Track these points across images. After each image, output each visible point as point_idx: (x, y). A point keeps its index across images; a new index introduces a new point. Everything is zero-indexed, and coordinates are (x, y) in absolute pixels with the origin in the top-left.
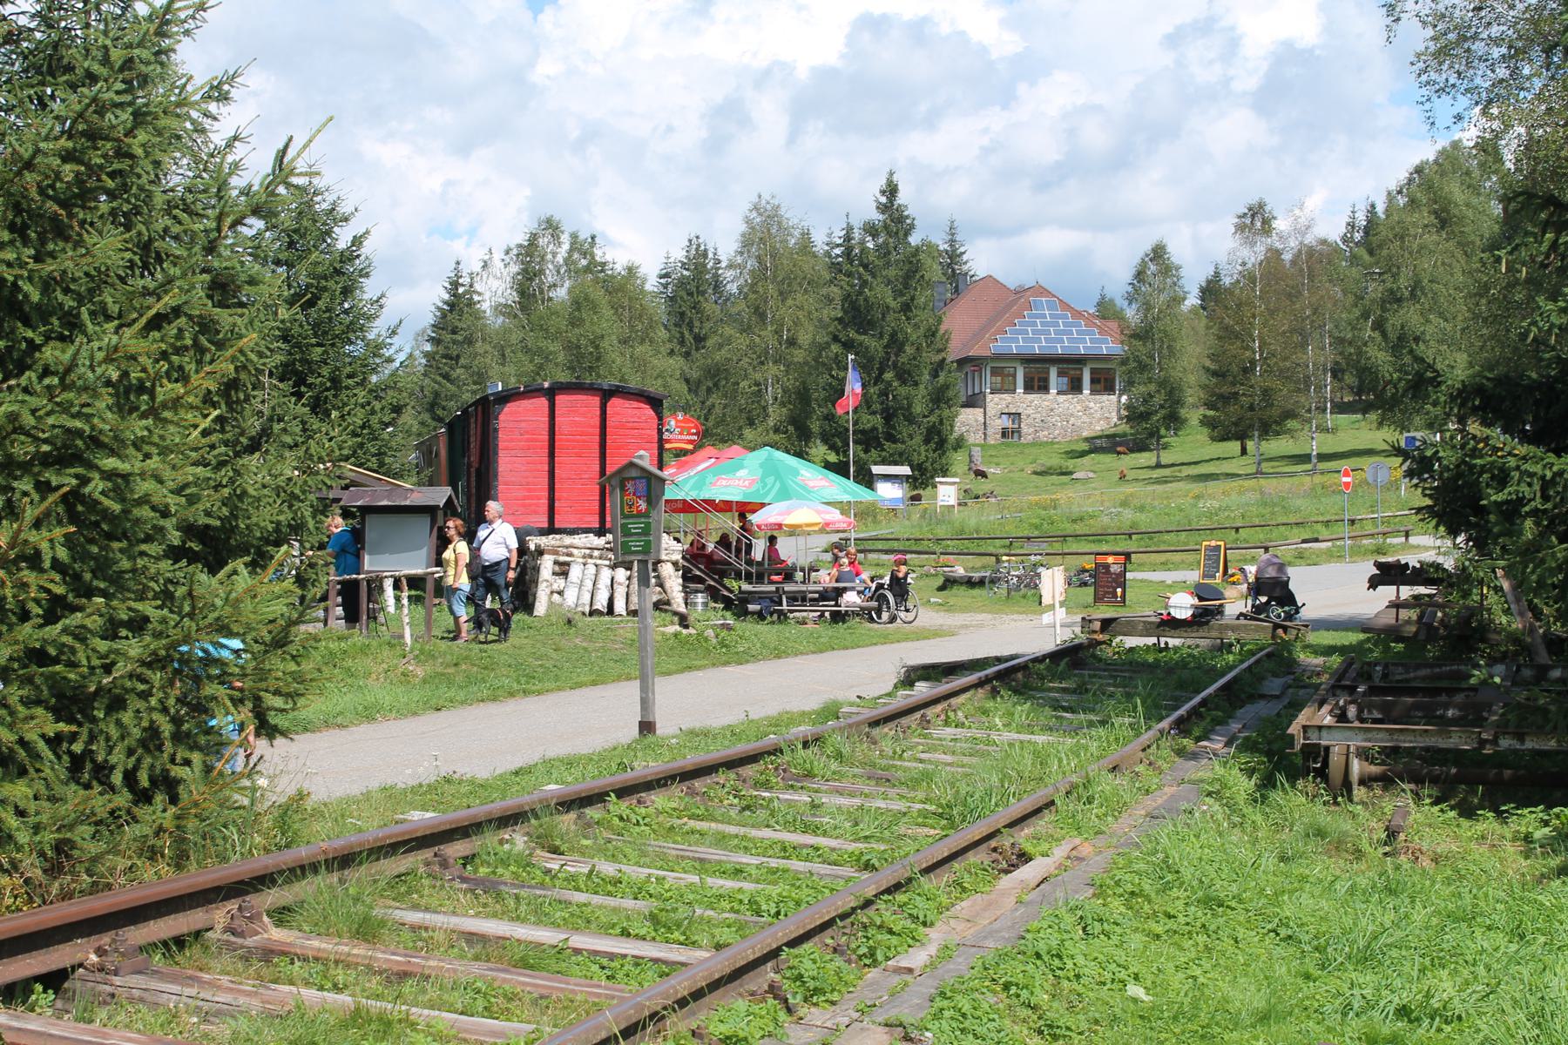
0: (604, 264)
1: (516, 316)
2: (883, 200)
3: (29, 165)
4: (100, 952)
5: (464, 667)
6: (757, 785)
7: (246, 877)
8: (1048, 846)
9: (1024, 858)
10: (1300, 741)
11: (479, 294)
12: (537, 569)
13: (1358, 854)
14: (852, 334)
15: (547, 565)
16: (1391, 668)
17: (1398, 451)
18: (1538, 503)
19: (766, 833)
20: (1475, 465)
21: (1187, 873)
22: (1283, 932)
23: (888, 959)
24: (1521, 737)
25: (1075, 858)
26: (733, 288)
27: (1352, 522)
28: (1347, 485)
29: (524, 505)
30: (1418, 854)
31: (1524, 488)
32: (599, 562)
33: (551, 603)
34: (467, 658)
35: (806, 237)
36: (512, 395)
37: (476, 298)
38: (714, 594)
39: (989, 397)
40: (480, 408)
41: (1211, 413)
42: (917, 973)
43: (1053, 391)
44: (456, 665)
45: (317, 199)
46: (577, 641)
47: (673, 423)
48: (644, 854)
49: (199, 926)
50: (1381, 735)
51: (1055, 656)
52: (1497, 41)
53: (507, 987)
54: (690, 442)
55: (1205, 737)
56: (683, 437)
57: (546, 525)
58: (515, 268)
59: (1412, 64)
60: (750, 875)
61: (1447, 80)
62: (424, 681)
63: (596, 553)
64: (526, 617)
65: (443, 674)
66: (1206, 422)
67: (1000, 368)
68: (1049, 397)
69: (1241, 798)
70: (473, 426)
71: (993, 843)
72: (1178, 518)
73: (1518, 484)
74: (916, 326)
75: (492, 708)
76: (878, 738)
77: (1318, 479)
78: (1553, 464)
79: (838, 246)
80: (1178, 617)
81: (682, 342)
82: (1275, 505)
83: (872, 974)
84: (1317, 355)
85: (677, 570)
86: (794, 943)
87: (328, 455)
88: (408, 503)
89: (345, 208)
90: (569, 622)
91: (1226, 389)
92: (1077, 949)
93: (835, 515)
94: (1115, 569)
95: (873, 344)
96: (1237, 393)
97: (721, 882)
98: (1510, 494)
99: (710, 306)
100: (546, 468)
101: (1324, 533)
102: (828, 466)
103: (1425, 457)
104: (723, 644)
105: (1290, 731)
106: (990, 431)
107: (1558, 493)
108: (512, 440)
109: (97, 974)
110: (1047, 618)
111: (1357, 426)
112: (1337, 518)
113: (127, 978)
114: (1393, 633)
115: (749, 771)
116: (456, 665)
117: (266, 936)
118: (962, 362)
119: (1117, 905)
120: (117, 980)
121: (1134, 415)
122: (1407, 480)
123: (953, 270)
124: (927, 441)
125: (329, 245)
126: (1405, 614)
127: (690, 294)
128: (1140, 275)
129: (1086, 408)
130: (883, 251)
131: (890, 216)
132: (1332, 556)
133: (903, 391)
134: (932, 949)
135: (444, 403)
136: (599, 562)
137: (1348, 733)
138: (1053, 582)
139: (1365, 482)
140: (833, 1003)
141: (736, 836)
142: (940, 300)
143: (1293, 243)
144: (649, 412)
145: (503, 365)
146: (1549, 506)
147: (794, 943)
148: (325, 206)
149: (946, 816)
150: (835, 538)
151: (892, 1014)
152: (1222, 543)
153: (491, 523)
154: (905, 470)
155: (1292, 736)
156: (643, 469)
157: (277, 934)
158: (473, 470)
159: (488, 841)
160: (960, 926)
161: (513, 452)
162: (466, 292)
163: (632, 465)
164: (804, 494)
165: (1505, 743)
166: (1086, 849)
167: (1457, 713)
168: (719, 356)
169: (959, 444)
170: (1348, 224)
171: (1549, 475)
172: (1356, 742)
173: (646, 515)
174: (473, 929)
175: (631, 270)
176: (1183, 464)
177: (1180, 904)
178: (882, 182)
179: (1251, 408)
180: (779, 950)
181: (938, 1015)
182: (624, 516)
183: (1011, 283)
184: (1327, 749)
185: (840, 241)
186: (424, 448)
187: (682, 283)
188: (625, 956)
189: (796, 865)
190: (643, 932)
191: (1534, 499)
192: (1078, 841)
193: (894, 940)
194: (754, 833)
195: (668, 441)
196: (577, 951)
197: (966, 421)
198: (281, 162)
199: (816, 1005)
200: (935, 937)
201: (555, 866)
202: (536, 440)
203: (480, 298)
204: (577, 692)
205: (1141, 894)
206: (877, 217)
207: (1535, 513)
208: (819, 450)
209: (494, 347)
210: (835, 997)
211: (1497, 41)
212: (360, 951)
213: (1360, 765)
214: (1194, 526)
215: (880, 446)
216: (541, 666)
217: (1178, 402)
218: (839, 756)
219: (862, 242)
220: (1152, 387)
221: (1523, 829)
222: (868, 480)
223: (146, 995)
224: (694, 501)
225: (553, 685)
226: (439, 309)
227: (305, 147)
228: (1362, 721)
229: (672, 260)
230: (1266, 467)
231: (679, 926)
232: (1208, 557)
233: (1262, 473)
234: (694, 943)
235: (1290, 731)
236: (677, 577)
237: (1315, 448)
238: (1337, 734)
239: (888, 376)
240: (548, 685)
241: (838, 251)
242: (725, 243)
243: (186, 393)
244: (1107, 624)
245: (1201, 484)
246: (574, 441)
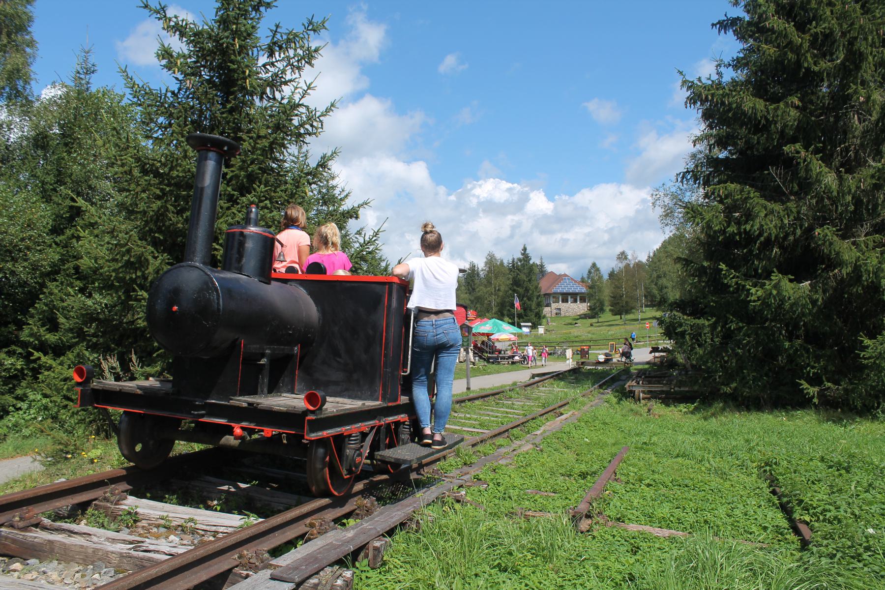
6: (499, 399)
9: (562, 414)
13: (641, 415)
14: (515, 288)
17: (658, 319)
18: (689, 331)
21: (599, 417)
26: (482, 276)
27: (649, 337)
35: (502, 263)
38: (480, 357)
51: (569, 371)
52: (680, 213)
55: (606, 389)
66: (611, 310)
67: (555, 296)
81: (469, 290)
84: (640, 292)
86: (512, 428)
91: (616, 302)
93: (513, 336)
94: (586, 350)
95: (521, 290)
101: (642, 340)
102: (509, 323)
104: (484, 370)
110: (568, 362)
114: (654, 364)
115: (497, 396)
118: (545, 295)
121: (591, 308)
124: (536, 316)
126: (656, 360)
128: (590, 272)
130: (523, 266)
133: (529, 303)
138: (569, 353)
143: (633, 262)
147: (512, 428)
149: (544, 406)
150: (511, 342)
151: (533, 442)
154: (530, 324)
164: (504, 331)
165: (676, 389)
166: (576, 413)
168: (479, 294)
169: (544, 317)
172: (641, 389)
178: (522, 247)
181: (543, 443)
189: (509, 415)
197: (546, 310)
200: (542, 429)
207: (689, 334)
208: (506, 319)
211: (680, 213)
215: (523, 318)
218: (518, 393)
222: (520, 327)
239: (525, 299)
242: (481, 264)
244: (583, 363)
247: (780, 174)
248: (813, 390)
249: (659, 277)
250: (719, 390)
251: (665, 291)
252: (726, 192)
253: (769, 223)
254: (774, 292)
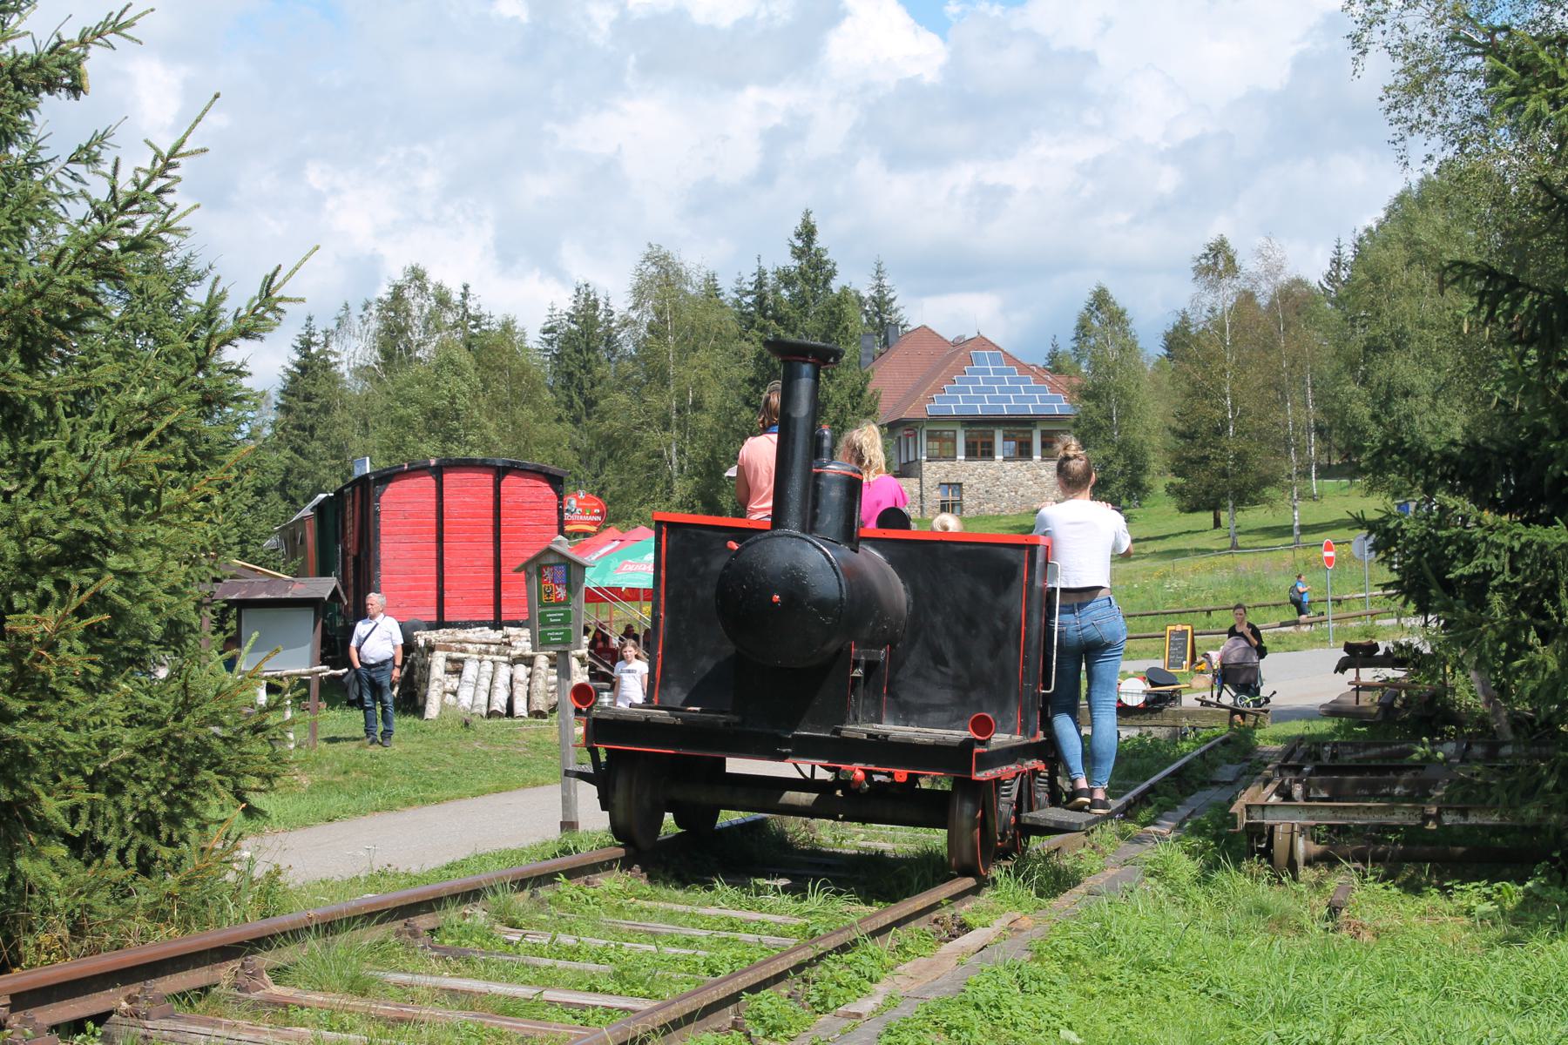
0: (477, 318)
1: (379, 380)
2: (799, 244)
3: (39, 295)
4: (131, 999)
5: (354, 775)
7: (245, 939)
8: (988, 918)
9: (965, 928)
10: (1243, 821)
11: (336, 355)
12: (427, 668)
13: (1300, 931)
15: (438, 662)
16: (1340, 747)
18: (1506, 576)
19: (713, 911)
20: (1441, 538)
22: (1214, 991)
23: (837, 1006)
24: (1464, 812)
25: (1014, 928)
28: (1329, 560)
29: (409, 596)
30: (1360, 929)
31: (1491, 560)
32: (496, 658)
33: (443, 706)
34: (356, 765)
35: (712, 291)
36: (395, 474)
37: (332, 359)
39: (926, 465)
40: (358, 489)
41: (1180, 480)
42: (865, 1018)
43: (999, 457)
44: (345, 773)
45: (167, 256)
46: (476, 745)
47: (574, 502)
48: (596, 928)
49: (204, 983)
50: (1324, 814)
53: (495, 1028)
54: (593, 523)
56: (586, 518)
57: (434, 619)
58: (375, 325)
59: (1381, 99)
60: (702, 944)
61: (1420, 116)
62: (311, 792)
63: (493, 648)
64: (417, 720)
65: (331, 783)
66: (1172, 490)
68: (995, 464)
69: (1184, 879)
70: (349, 508)
71: (935, 915)
72: (1142, 600)
73: (1485, 557)
74: (840, 386)
75: (388, 818)
76: (816, 826)
77: (1300, 554)
78: (1521, 535)
79: (749, 293)
80: (1130, 704)
81: (570, 406)
82: (1248, 584)
83: (824, 1018)
84: (1300, 413)
85: (583, 666)
86: (754, 989)
87: (211, 544)
88: (289, 595)
89: (197, 266)
90: (467, 724)
91: (1193, 453)
92: (1015, 999)
96: (1207, 458)
97: (675, 950)
98: (1477, 567)
99: (605, 370)
100: (434, 554)
103: (1389, 530)
105: (1232, 810)
106: (927, 505)
107: (1527, 565)
108: (396, 524)
109: (130, 1019)
111: (1346, 492)
112: (1321, 597)
113: (157, 1022)
116: (345, 773)
117: (267, 991)
119: (1054, 967)
120: (149, 1024)
122: (1374, 553)
123: (882, 320)
125: (180, 307)
127: (579, 351)
128: (1083, 329)
129: (1037, 477)
130: (801, 303)
131: (808, 261)
132: (1314, 641)
134: (879, 999)
135: (296, 481)
136: (496, 658)
137: (1293, 812)
139: (1351, 557)
140: (790, 1039)
141: (684, 913)
142: (867, 355)
144: (547, 490)
145: (366, 436)
146: (1518, 579)
147: (754, 989)
148: (175, 263)
152: (1189, 628)
153: (372, 618)
155: (1234, 816)
156: (562, 555)
157: (276, 990)
158: (350, 558)
159: (452, 915)
160: (904, 983)
161: (397, 538)
162: (320, 352)
163: (550, 551)
166: (1026, 922)
167: (1404, 791)
170: (1333, 261)
171: (1517, 545)
173: (566, 603)
174: (448, 986)
175: (507, 327)
176: (1148, 539)
177: (1115, 969)
179: (1224, 474)
180: (739, 993)
182: (543, 605)
183: (950, 337)
184: (1272, 827)
185: (750, 288)
186: (287, 534)
187: (569, 338)
188: (595, 1007)
189: (743, 936)
190: (609, 987)
191: (1502, 572)
192: (1017, 915)
193: (842, 991)
194: (701, 911)
195: (569, 523)
196: (552, 1003)
198: (269, 287)
199: (775, 1040)
200: (880, 992)
201: (516, 938)
202: (422, 524)
203: (337, 360)
204: (480, 799)
205: (1077, 958)
206: (792, 263)
209: (355, 416)
210: (793, 1033)
212: (357, 1002)
213: (1306, 845)
214: (1160, 610)
216: (439, 772)
219: (776, 291)
220: (1109, 452)
221: (1464, 903)
223: (176, 1036)
224: (598, 589)
225: (453, 793)
226: (289, 372)
227: (291, 274)
228: (1307, 799)
229: (557, 312)
230: (1240, 540)
231: (642, 982)
232: (1173, 644)
233: (1238, 548)
234: (657, 996)
235: (1232, 810)
236: (583, 673)
237: (1297, 518)
238: (1280, 813)
240: (447, 793)
241: (749, 299)
243: (191, 500)
245: (1169, 562)
246: (464, 524)
251: (1401, 406)
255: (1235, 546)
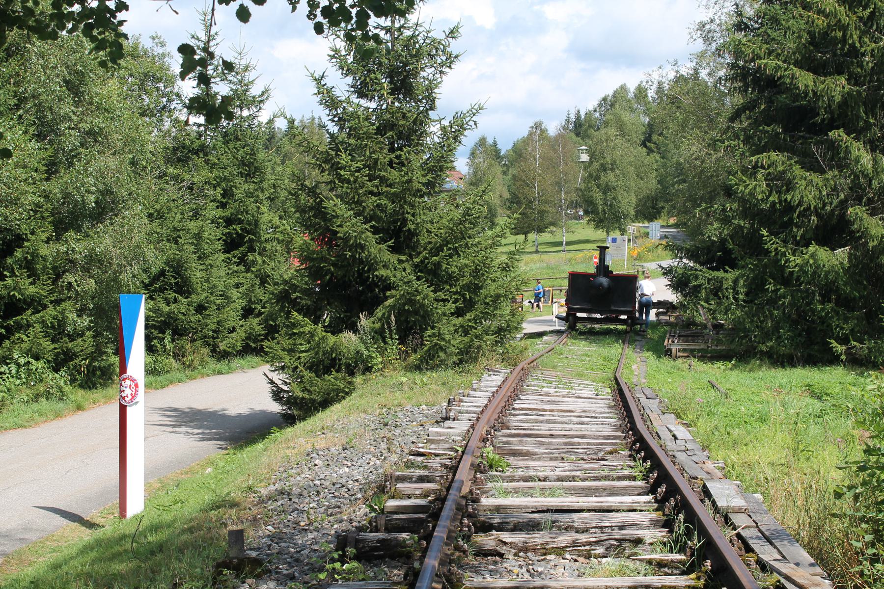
31: (703, 281)
170: (566, 120)
217: (494, 215)
230: (541, 248)
247: (821, 153)
248: (840, 348)
249: (603, 168)
250: (755, 348)
252: (769, 162)
253: (795, 24)
254: (811, 261)
255: (537, 252)
